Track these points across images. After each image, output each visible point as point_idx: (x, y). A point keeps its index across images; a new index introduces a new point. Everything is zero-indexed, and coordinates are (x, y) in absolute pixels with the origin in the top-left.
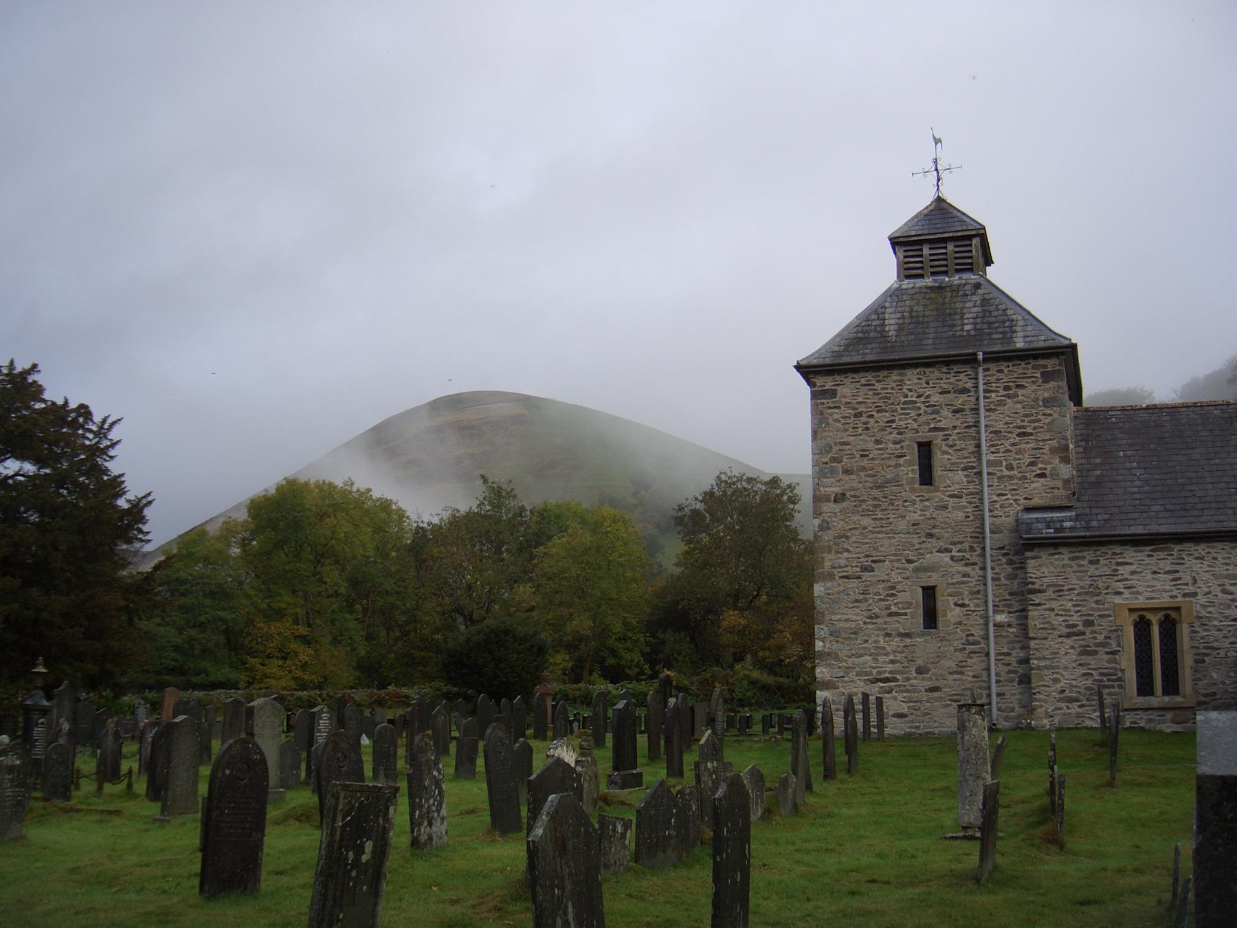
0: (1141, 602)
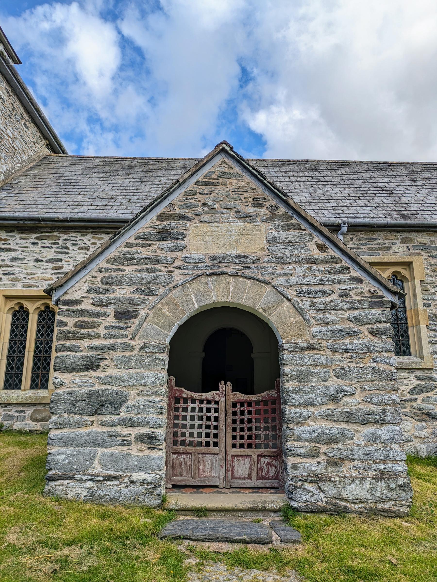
0: (18, 289)
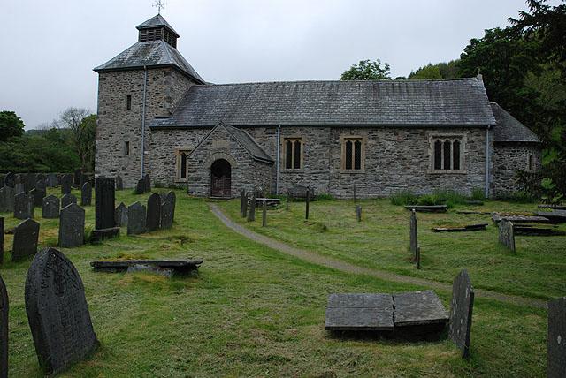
0: (182, 148)
